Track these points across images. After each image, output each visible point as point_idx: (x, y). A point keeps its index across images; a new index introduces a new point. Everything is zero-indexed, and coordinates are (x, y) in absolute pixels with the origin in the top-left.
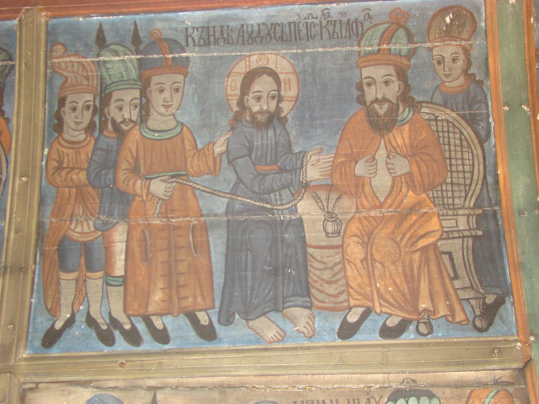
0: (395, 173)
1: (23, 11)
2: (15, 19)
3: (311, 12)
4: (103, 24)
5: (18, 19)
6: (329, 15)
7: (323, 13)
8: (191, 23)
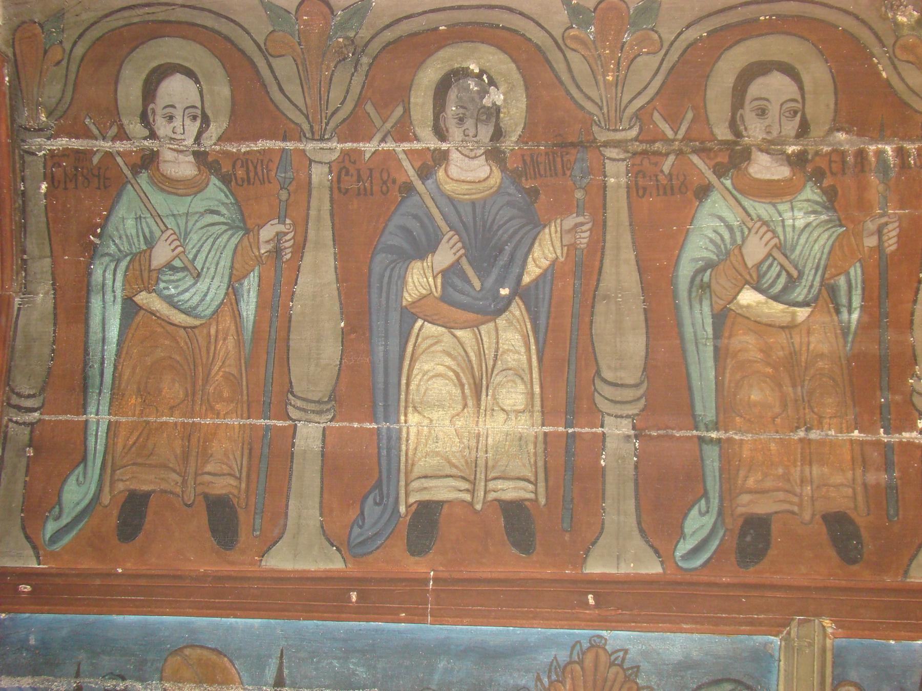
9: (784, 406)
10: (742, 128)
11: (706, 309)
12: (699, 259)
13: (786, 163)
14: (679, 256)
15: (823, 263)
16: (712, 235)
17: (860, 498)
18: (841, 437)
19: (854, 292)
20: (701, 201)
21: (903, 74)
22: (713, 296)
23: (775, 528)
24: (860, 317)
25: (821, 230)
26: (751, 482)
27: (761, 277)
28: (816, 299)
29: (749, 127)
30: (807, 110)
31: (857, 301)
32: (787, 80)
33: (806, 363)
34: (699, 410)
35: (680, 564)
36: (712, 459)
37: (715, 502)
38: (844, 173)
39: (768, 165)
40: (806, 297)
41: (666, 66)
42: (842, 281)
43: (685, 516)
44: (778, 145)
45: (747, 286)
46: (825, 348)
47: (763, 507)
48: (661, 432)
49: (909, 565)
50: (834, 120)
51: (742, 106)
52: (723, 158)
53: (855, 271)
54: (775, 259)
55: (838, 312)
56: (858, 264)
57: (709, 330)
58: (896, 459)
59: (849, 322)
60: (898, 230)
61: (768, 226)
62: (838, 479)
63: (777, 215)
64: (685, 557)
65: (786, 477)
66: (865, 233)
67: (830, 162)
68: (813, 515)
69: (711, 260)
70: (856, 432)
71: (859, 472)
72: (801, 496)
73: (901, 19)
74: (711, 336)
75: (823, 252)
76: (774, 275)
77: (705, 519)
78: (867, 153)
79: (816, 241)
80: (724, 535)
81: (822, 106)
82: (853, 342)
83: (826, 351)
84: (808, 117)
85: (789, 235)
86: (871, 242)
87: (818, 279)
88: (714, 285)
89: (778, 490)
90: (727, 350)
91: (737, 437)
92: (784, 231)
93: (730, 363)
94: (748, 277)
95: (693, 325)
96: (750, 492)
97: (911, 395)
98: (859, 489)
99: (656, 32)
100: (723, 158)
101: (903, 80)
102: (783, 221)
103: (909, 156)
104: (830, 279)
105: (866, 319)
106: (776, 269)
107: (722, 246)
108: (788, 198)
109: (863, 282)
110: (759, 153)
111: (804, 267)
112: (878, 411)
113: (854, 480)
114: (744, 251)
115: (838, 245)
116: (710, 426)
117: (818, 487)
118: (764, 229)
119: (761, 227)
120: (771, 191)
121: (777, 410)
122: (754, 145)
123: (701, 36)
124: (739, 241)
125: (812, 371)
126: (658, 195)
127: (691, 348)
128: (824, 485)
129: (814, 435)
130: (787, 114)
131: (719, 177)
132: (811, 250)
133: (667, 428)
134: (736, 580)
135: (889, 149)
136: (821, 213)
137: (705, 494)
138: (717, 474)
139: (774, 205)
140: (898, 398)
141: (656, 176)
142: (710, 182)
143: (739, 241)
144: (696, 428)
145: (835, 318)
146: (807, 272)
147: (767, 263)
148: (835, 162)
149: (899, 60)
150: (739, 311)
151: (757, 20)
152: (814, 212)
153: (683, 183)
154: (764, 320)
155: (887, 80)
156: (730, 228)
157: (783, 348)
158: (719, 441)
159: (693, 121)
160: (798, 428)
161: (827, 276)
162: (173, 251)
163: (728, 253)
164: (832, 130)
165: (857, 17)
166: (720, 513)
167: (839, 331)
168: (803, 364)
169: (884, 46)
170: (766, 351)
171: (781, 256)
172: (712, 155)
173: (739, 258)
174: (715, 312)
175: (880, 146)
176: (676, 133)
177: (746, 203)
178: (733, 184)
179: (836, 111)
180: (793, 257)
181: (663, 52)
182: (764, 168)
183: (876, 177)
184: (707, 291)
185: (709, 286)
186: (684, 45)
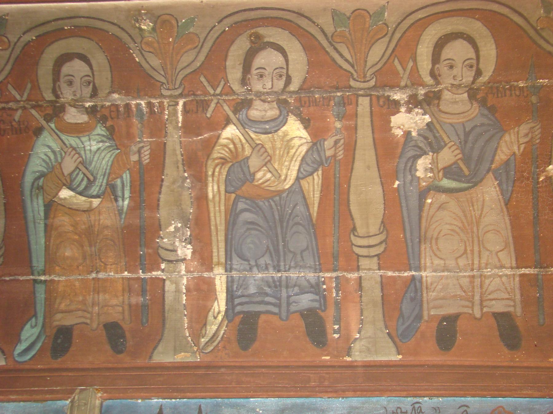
0: (450, 148)
1: (77, 391)
2: (67, 400)
3: (401, 406)
4: (163, 408)
5: (70, 400)
6: (421, 410)
7: (414, 407)
8: (263, 410)
9: (84, 258)
10: (59, 93)
11: (41, 202)
12: (37, 172)
13: (85, 113)
14: (25, 170)
15: (108, 171)
16: (44, 157)
17: (127, 313)
18: (117, 276)
19: (125, 189)
20: (37, 137)
21: (148, 59)
22: (45, 194)
23: (75, 333)
24: (129, 203)
25: (106, 152)
26: (63, 307)
27: (72, 181)
28: (104, 193)
29: (63, 92)
30: (96, 81)
31: (127, 194)
32: (83, 64)
33: (98, 232)
34: (35, 264)
35: (17, 359)
36: (41, 294)
37: (41, 319)
38: (118, 118)
39: (75, 114)
40: (98, 192)
41: (14, 56)
42: (119, 182)
43: (22, 329)
44: (81, 102)
45: (64, 187)
46: (108, 222)
47: (68, 321)
48: (12, 278)
49: (152, 353)
50: (111, 87)
51: (58, 80)
52: (50, 111)
53: (126, 176)
54: (80, 170)
55: (116, 200)
56: (128, 172)
57: (42, 214)
58: (148, 288)
59: (123, 207)
60: (149, 151)
61: (76, 150)
62: (114, 302)
63: (81, 144)
64: (20, 354)
65: (84, 302)
66: (131, 153)
67: (111, 111)
68: (99, 324)
69: (43, 172)
70: (126, 273)
71: (126, 297)
72: (91, 313)
73: (143, 27)
74: (43, 218)
75: (107, 165)
76: (80, 180)
77: (35, 329)
78: (131, 105)
79: (103, 159)
80: (45, 340)
81: (104, 78)
82: (125, 218)
83: (109, 225)
84: (97, 85)
85: (88, 155)
86: (134, 158)
87: (105, 181)
88: (45, 187)
89: (79, 310)
90: (52, 225)
91: (56, 279)
92: (85, 153)
93: (54, 233)
94: (65, 182)
95: (33, 211)
96: (62, 312)
97: (158, 249)
98: (126, 308)
99: (6, 37)
100: (50, 111)
101: (148, 62)
102: (84, 147)
103: (154, 107)
104: (112, 181)
105: (132, 204)
106: (81, 176)
107: (50, 164)
108: (88, 133)
109: (131, 182)
110: (70, 107)
111: (97, 174)
112: (139, 260)
113: (123, 302)
114: (63, 166)
115: (116, 160)
116: (41, 272)
117: (102, 307)
118: (74, 152)
119: (72, 151)
120: (78, 130)
121: (81, 261)
122: (67, 103)
123: (32, 39)
124: (59, 160)
125: (101, 237)
126: (13, 134)
127: (31, 225)
128: (106, 306)
129: (101, 275)
130: (85, 84)
131: (48, 122)
132: (101, 164)
133: (16, 275)
134: (46, 367)
135: (143, 103)
136: (106, 142)
137: (35, 315)
138: (43, 302)
139: (79, 138)
140: (150, 251)
141: (11, 122)
142: (42, 126)
143: (59, 160)
144: (33, 274)
145: (115, 204)
146: (98, 177)
147: (76, 173)
148: (113, 111)
149: (145, 51)
150: (59, 202)
151: (63, 29)
152: (102, 141)
153: (27, 127)
154: (74, 207)
155: (139, 62)
156: (54, 152)
157: (84, 224)
158: (46, 281)
159: (31, 90)
160: (92, 272)
161: (110, 179)
162: (456, 156)
163: (53, 168)
164: (110, 93)
165: (119, 27)
166: (43, 326)
167: (117, 212)
168: (96, 233)
169: (136, 43)
170: (75, 225)
171: (84, 169)
172: (43, 109)
173: (60, 170)
174: (46, 203)
175: (138, 102)
176: (22, 97)
177: (63, 137)
178: (56, 127)
179: (112, 82)
180: (90, 169)
181: (10, 49)
182: (73, 116)
183: (136, 120)
184: (41, 190)
185: (42, 188)
186: (23, 44)
